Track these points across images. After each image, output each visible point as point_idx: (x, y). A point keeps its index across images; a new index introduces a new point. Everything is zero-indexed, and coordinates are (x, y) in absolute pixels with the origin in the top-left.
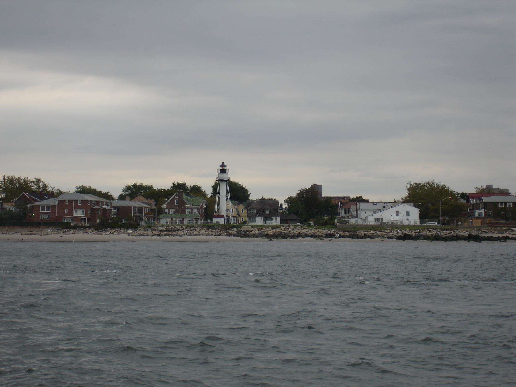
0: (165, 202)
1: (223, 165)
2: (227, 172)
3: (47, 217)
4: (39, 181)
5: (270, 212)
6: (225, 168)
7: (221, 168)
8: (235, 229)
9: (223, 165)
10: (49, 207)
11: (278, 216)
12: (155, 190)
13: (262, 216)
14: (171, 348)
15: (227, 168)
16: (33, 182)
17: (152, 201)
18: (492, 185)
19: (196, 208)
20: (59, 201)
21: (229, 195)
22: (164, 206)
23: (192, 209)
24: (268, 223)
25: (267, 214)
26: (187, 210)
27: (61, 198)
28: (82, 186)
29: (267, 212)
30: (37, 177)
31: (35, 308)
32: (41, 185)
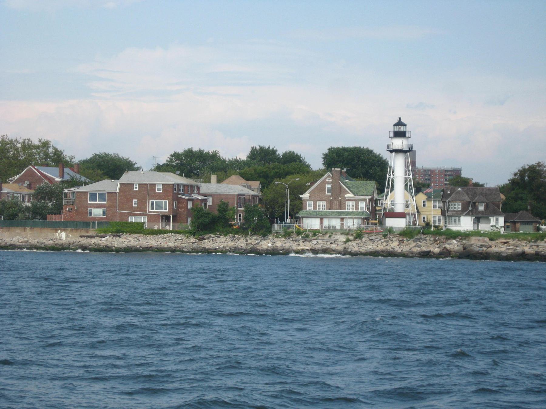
0: (309, 187)
1: (400, 123)
2: (407, 135)
3: (98, 213)
4: (46, 144)
5: (487, 207)
6: (402, 129)
7: (397, 129)
8: (454, 241)
9: (400, 123)
10: (102, 196)
11: (500, 215)
12: (224, 161)
13: (472, 215)
14: (9, 390)
15: (408, 129)
16: (37, 147)
17: (256, 184)
18: (192, 148)
19: (364, 200)
20: (121, 184)
21: (388, 176)
22: (306, 196)
23: (357, 201)
24: (484, 227)
25: (136, 191)
26: (347, 203)
27: (127, 178)
28: (176, 156)
29: (481, 208)
30: (45, 138)
31: (49, 377)
32: (51, 150)
